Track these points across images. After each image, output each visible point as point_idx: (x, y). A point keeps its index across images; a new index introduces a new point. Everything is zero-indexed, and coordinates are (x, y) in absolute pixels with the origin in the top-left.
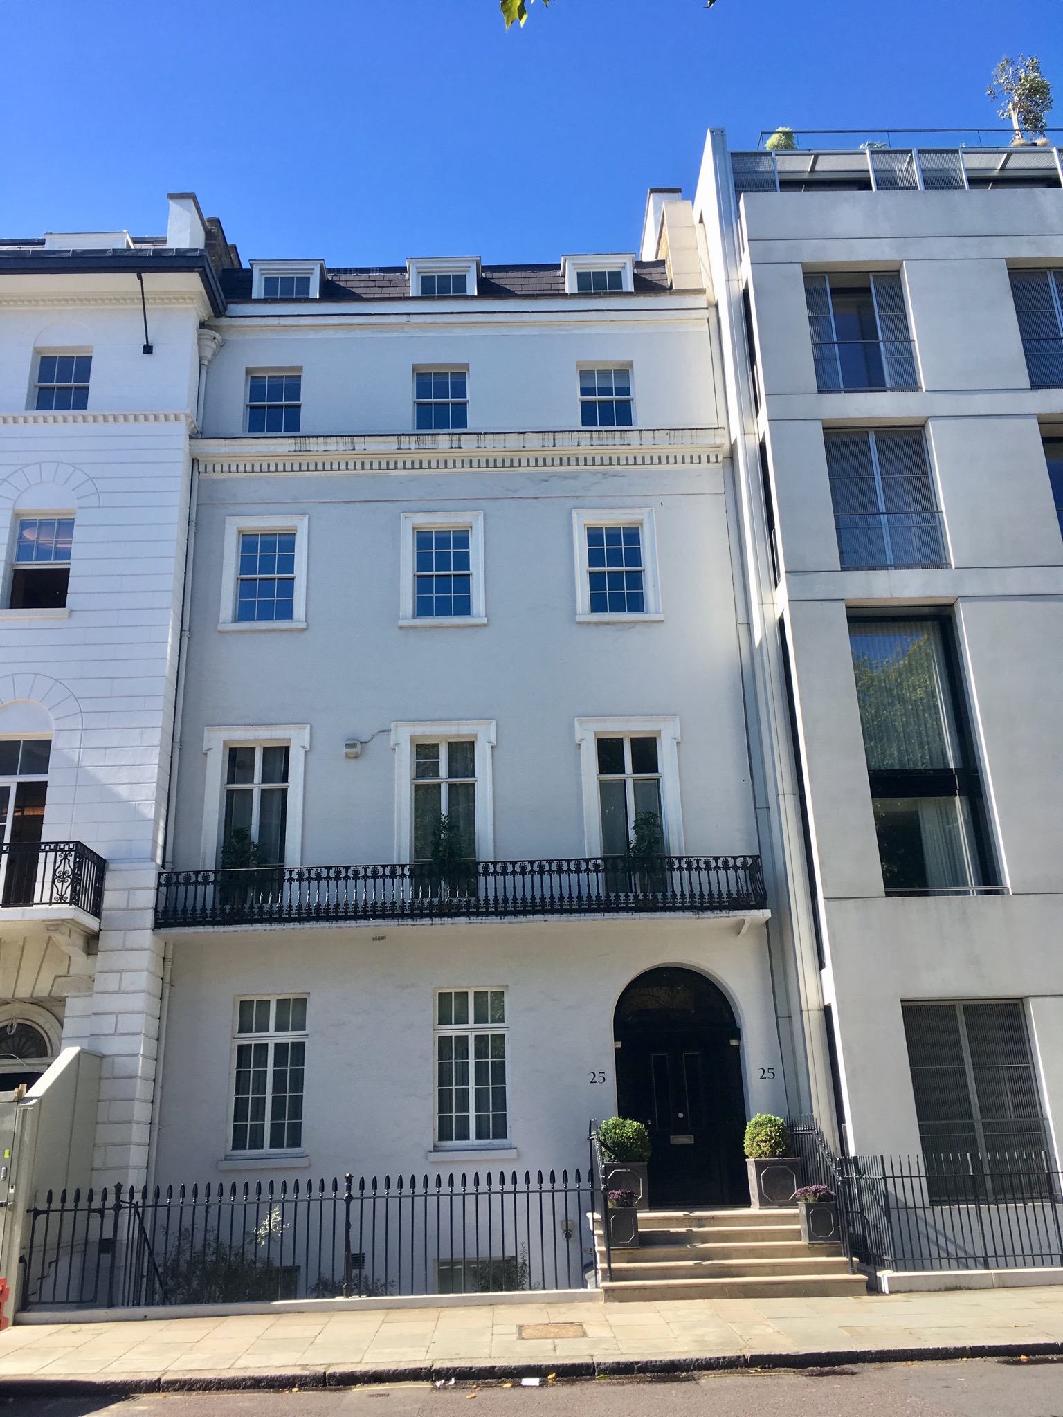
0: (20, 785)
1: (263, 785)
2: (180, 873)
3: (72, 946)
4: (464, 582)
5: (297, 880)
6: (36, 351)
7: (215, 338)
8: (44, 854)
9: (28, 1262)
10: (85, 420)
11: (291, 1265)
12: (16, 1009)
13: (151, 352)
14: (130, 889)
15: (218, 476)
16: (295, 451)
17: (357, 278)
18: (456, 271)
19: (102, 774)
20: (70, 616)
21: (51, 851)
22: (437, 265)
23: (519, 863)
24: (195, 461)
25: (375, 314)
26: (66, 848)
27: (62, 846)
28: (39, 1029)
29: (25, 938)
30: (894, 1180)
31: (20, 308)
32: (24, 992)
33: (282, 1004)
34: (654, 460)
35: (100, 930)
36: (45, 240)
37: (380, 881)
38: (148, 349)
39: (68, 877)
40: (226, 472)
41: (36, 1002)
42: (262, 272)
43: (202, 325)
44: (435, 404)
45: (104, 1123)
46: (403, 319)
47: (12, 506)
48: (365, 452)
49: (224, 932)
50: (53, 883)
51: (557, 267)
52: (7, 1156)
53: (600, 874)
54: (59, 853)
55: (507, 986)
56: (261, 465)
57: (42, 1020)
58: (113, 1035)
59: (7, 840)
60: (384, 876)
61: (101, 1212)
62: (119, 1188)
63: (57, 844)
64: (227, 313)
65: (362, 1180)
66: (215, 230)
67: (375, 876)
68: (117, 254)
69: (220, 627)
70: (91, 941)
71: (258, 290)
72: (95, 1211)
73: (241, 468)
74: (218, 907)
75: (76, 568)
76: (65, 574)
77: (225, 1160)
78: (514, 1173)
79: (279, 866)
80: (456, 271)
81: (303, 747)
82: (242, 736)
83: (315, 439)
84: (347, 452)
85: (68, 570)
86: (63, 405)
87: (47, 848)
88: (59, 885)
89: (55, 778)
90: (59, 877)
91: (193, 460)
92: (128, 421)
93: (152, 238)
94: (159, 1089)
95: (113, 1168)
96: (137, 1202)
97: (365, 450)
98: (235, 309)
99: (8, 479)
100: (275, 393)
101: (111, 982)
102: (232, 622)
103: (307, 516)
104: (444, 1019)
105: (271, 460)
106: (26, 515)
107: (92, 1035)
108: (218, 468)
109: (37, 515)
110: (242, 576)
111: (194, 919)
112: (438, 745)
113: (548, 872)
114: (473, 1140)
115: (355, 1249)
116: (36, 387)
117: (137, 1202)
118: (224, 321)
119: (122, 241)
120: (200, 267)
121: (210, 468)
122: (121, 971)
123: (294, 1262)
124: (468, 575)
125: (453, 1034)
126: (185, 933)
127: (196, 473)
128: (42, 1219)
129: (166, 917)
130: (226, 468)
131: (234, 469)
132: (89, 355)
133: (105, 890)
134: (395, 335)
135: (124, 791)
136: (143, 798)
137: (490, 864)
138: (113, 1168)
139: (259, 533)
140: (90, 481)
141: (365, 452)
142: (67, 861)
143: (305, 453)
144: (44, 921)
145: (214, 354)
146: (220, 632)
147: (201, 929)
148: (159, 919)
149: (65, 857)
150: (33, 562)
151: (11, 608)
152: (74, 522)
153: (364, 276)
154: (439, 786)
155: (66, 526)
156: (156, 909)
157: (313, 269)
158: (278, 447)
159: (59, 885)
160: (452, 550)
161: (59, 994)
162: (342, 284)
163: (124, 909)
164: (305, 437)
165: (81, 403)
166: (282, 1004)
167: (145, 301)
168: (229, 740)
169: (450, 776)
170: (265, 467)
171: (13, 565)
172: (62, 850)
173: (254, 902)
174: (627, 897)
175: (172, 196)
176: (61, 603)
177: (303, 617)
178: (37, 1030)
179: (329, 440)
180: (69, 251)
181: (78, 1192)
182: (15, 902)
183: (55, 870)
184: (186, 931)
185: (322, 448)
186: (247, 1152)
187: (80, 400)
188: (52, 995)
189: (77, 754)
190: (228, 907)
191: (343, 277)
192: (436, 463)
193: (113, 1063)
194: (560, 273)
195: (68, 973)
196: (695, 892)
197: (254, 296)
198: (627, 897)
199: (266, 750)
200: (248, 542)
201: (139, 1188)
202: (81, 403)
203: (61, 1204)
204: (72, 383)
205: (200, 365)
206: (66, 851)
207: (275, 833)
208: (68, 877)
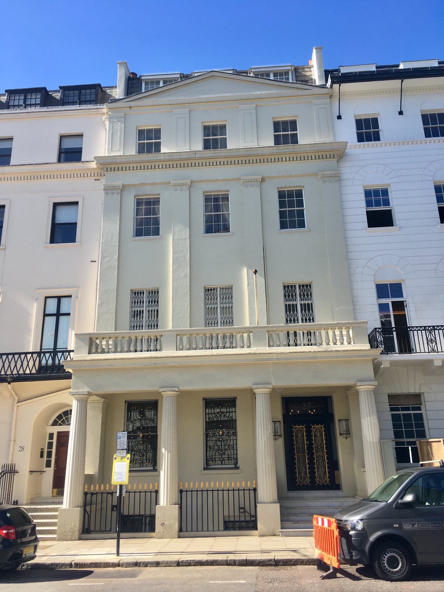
0: (393, 302)
9: (89, 515)
11: (128, 514)
21: (423, 330)
27: (427, 328)
38: (339, 117)
50: (428, 344)
59: (393, 325)
63: (425, 327)
68: (432, 69)
87: (421, 329)
88: (431, 345)
115: (242, 505)
123: (134, 513)
167: (402, 92)
172: (428, 330)
182: (405, 352)
183: (427, 339)
206: (430, 330)
207: (246, 330)
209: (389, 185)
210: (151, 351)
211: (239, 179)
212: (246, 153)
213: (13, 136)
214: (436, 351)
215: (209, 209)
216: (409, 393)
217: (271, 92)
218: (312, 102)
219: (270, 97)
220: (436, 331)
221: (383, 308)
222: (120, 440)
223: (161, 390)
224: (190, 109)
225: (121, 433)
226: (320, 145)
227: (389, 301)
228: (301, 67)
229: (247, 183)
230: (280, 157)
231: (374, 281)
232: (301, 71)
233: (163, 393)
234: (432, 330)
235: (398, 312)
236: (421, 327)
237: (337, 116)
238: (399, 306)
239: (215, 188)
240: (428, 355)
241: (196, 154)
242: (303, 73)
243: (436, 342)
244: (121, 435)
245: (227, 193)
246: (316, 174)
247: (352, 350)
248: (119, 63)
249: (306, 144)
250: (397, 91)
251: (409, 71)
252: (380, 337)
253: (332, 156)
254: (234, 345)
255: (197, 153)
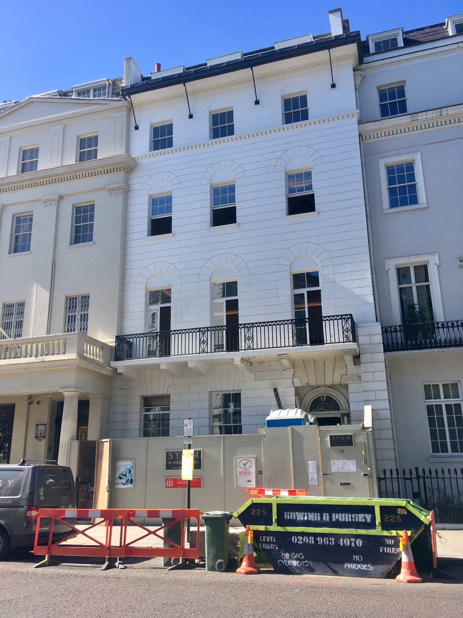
0: (308, 292)
1: (416, 284)
2: (439, 323)
3: (349, 360)
4: (413, 188)
5: (451, 327)
6: (151, 125)
7: (361, 75)
8: (184, 334)
10: (310, 124)
12: (322, 389)
13: (335, 87)
14: (370, 335)
15: (372, 140)
16: (411, 121)
17: (418, 34)
18: (384, 38)
19: (345, 284)
20: (318, 214)
22: (456, 19)
23: (440, 323)
24: (360, 135)
25: (440, 47)
26: (249, 326)
27: (202, 329)
28: (334, 398)
29: (325, 358)
30: (431, 480)
31: (273, 79)
32: (329, 382)
33: (445, 386)
34: (456, 121)
35: (360, 354)
36: (207, 63)
37: (456, 329)
38: (137, 128)
39: (350, 330)
40: (376, 138)
41: (332, 387)
42: (373, 40)
43: (354, 70)
44: (398, 102)
45: (378, 439)
46: (456, 46)
47: (284, 169)
48: (448, 115)
49: (418, 353)
50: (200, 345)
51: (444, 24)
52: (363, 453)
53: (445, 329)
54: (201, 332)
55: (460, 381)
56: (393, 132)
57: (336, 395)
58: (375, 400)
59: (307, 316)
60: (448, 327)
61: (411, 479)
62: (417, 469)
64: (364, 62)
65: (424, 470)
66: (347, 25)
67: (453, 326)
69: (384, 212)
70: (357, 358)
71: (372, 50)
72: (407, 479)
73: (383, 135)
74: (404, 342)
75: (175, 215)
76: (312, 196)
77: (431, 457)
78: (436, 470)
79: (431, 322)
80: (384, 38)
81: (436, 264)
82: (403, 262)
83: (421, 113)
84: (438, 117)
85: (235, 207)
86: (224, 135)
88: (248, 342)
89: (322, 287)
90: (247, 338)
91: (359, 135)
92: (307, 126)
93: (319, 35)
94: (394, 425)
95: (387, 460)
96: (427, 476)
97: (447, 114)
98: (366, 59)
99: (281, 158)
100: (392, 96)
101: (369, 377)
102: (390, 209)
103: (420, 152)
104: (428, 397)
105: (442, 120)
106: (290, 172)
107: (365, 401)
108: (372, 137)
109: (295, 171)
110: (390, 186)
111: (402, 348)
112: (409, 267)
113: (456, 326)
114: (450, 453)
116: (212, 129)
117: (427, 476)
118: (363, 66)
119: (309, 39)
120: (358, 40)
121: (368, 137)
122: (374, 372)
124: (415, 185)
125: (434, 404)
126: (399, 354)
127: (361, 141)
128: (383, 482)
129: (388, 347)
130: (376, 136)
131: (379, 136)
132: (171, 123)
133: (359, 336)
134: (452, 55)
135: (357, 291)
136: (367, 294)
137: (397, 327)
138: (387, 460)
139: (395, 165)
140: (240, 166)
141: (448, 115)
142: (348, 323)
143: (416, 121)
144: (342, 350)
145: (361, 83)
146: (385, 214)
147: (406, 352)
148: (385, 348)
149: (204, 334)
150: (221, 205)
151: (214, 226)
152: (235, 186)
153: (422, 32)
154: (411, 287)
155: (308, 175)
156: (383, 343)
157: (398, 33)
158: (401, 121)
159: (248, 342)
160: (396, 175)
161: (344, 383)
162: (411, 38)
163: (369, 344)
164: (415, 113)
165: (231, 132)
166: (445, 386)
168: (397, 264)
169: (416, 283)
170: (395, 132)
171: (288, 196)
173: (422, 339)
174: (431, 341)
175: (331, 12)
176: (313, 210)
177: (425, 201)
178: (333, 399)
179: (428, 112)
180: (295, 46)
181: (391, 471)
183: (200, 340)
184: (399, 353)
185: (424, 117)
186: (440, 454)
187: (305, 116)
188: (342, 382)
189: (333, 276)
190: (409, 342)
191: (411, 34)
192: (454, 121)
193: (378, 413)
194: (445, 27)
195: (347, 373)
196: (389, 343)
197: (371, 52)
198: (431, 341)
199: (416, 268)
200: (390, 170)
201: (394, 468)
202: (231, 132)
203: (436, 475)
204: (292, 111)
205: (355, 89)
208: (350, 330)
209: (171, 192)
210: (17, 357)
211: (40, 200)
212: (44, 175)
213: (233, 106)
214: (252, 348)
215: (24, 229)
216: (158, 394)
217: (78, 111)
218: (112, 116)
219: (75, 116)
220: (254, 329)
221: (298, 299)
222: (186, 427)
223: (60, 391)
224: (11, 137)
225: (187, 420)
226: (104, 160)
227: (304, 291)
228: (119, 79)
229: (47, 202)
230: (75, 174)
231: (289, 272)
232: (118, 83)
233: (64, 393)
234: (250, 327)
235: (233, 312)
236: (337, 316)
237: (331, 85)
238: (315, 296)
239: (83, 200)
240: (198, 356)
241: (4, 180)
242: (120, 85)
243: (207, 343)
244: (187, 422)
245: (93, 203)
246: (103, 189)
247: (55, 360)
248: (125, 59)
249: (101, 159)
250: (326, 63)
251: (294, 48)
252: (346, 325)
253: (118, 169)
254: (18, 355)
255: (5, 179)
